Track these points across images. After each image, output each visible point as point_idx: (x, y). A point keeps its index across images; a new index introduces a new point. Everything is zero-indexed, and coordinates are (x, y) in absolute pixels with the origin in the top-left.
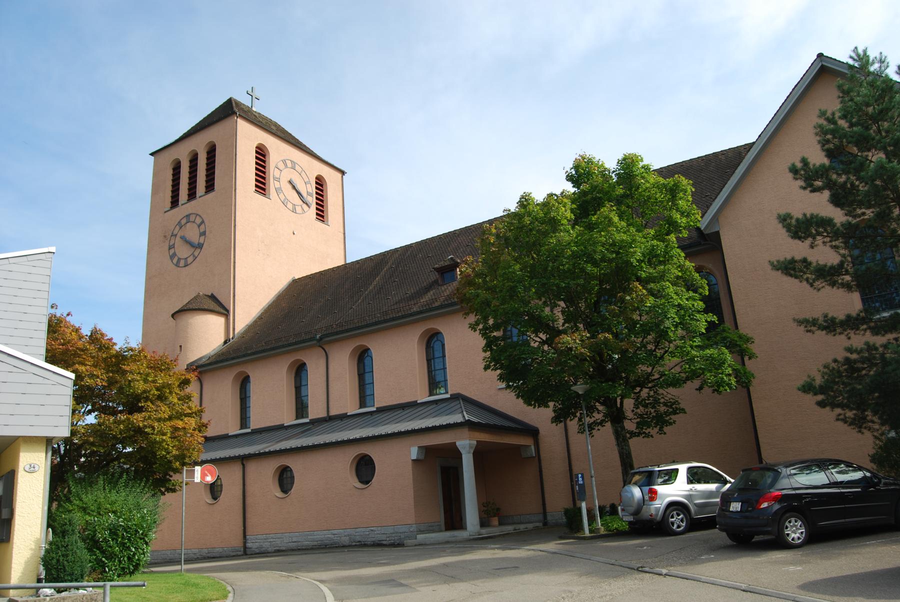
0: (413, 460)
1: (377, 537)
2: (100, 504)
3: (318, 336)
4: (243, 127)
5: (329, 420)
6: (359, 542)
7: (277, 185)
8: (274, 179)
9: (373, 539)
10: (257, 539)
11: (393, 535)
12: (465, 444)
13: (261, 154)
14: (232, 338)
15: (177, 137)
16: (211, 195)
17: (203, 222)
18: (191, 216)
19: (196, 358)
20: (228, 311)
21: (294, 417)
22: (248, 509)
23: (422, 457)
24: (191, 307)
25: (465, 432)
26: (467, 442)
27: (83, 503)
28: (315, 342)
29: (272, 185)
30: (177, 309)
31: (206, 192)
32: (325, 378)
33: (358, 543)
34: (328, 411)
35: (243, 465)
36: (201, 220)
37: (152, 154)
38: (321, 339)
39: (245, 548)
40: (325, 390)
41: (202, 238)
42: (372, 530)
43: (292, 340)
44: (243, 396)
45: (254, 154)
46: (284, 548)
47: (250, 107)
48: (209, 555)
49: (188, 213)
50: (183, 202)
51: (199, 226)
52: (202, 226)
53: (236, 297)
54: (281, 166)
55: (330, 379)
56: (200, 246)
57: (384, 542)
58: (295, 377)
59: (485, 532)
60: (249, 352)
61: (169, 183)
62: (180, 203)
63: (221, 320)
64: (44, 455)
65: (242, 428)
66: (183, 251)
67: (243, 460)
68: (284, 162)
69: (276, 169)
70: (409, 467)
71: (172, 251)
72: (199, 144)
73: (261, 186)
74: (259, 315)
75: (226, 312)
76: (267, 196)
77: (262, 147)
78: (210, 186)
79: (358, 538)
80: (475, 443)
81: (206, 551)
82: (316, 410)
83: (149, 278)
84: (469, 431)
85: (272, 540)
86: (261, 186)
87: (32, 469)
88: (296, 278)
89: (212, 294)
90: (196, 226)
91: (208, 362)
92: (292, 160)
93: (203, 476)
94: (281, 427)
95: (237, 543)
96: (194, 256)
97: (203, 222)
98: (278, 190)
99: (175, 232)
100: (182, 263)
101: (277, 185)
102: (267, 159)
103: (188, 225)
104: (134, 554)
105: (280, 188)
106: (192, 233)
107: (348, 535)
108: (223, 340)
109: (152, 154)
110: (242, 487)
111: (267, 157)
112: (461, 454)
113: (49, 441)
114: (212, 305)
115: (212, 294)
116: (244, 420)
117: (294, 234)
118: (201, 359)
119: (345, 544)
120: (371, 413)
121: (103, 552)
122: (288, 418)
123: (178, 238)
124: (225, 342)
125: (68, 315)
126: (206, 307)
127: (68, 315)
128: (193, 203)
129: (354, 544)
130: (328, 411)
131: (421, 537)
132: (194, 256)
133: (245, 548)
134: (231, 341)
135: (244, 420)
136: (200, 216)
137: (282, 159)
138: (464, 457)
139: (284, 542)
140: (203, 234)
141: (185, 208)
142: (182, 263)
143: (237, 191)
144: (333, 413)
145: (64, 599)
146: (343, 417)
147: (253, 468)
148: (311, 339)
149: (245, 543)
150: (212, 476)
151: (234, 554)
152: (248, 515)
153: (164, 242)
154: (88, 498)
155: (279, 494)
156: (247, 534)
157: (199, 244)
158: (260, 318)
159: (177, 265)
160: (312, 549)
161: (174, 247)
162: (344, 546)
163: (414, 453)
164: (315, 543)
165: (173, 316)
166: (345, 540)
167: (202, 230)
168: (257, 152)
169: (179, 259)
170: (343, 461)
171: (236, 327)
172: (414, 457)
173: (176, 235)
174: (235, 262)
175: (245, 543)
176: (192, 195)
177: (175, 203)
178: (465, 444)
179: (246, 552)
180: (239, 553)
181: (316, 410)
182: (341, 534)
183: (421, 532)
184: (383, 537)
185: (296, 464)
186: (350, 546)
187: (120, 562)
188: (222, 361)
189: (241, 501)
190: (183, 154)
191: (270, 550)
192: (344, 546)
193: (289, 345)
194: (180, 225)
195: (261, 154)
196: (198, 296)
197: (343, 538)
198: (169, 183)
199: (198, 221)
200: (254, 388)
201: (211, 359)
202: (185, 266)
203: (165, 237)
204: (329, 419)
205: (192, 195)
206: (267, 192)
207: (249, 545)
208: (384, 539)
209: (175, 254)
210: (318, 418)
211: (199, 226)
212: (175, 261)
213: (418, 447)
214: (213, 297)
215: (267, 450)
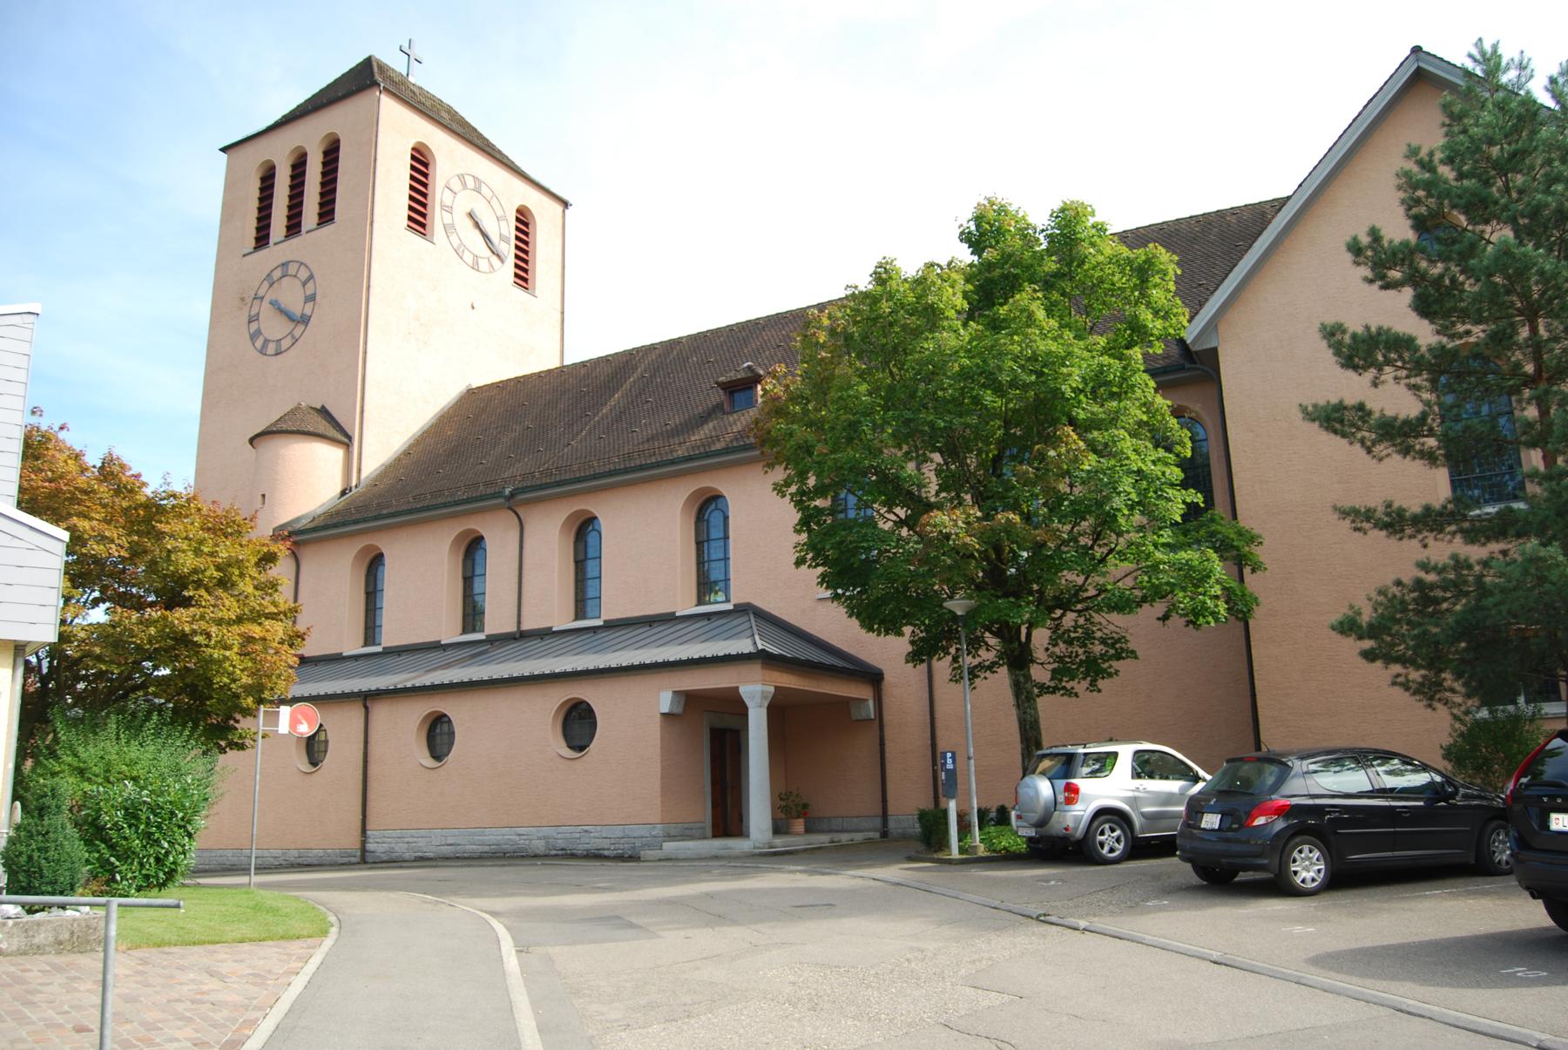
0: (662, 714)
3: (507, 491)
4: (391, 111)
6: (562, 849)
7: (447, 218)
8: (442, 207)
9: (587, 846)
10: (384, 837)
11: (623, 841)
12: (756, 690)
13: (421, 162)
14: (356, 487)
17: (311, 277)
20: (350, 438)
21: (460, 629)
23: (678, 710)
25: (756, 669)
28: (502, 500)
30: (259, 430)
31: (318, 224)
33: (560, 852)
34: (519, 622)
35: (366, 708)
36: (308, 274)
37: (224, 150)
38: (512, 495)
39: (364, 850)
42: (586, 831)
44: (371, 590)
45: (408, 161)
46: (431, 855)
48: (300, 861)
49: (284, 260)
51: (304, 284)
52: (310, 285)
53: (365, 414)
54: (456, 184)
55: (525, 567)
56: (305, 320)
59: (781, 843)
63: (334, 454)
64: (10, 671)
65: (366, 644)
66: (274, 327)
67: (367, 698)
68: (461, 177)
70: (658, 718)
71: (254, 326)
72: (310, 136)
73: (419, 218)
75: (346, 440)
76: (427, 237)
77: (423, 150)
78: (327, 214)
79: (561, 844)
80: (772, 689)
82: (497, 620)
84: (763, 668)
85: (411, 840)
86: (419, 218)
89: (323, 407)
90: (299, 284)
93: (294, 722)
95: (351, 842)
96: (293, 337)
97: (311, 277)
98: (449, 229)
99: (261, 293)
100: (271, 348)
101: (447, 218)
104: (167, 853)
105: (452, 226)
106: (292, 297)
107: (544, 838)
108: (339, 489)
109: (224, 150)
110: (362, 746)
111: (430, 167)
112: (746, 708)
114: (322, 426)
115: (323, 407)
116: (371, 631)
117: (473, 308)
118: (298, 519)
119: (538, 852)
120: (594, 629)
123: (266, 303)
124: (343, 493)
125: (62, 428)
126: (311, 430)
127: (62, 428)
128: (295, 241)
129: (554, 852)
130: (519, 622)
131: (669, 846)
132: (293, 337)
133: (364, 850)
134: (354, 491)
135: (371, 631)
136: (307, 267)
140: (311, 298)
141: (280, 249)
142: (271, 348)
143: (375, 225)
144: (527, 625)
145: (39, 924)
146: (545, 634)
149: (364, 843)
152: (371, 796)
153: (241, 309)
154: (89, 753)
155: (429, 762)
158: (407, 453)
159: (263, 351)
161: (258, 319)
163: (665, 702)
164: (486, 848)
165: (251, 441)
166: (539, 846)
167: (309, 292)
168: (413, 158)
169: (266, 341)
171: (363, 468)
175: (364, 843)
176: (294, 227)
177: (262, 239)
178: (756, 690)
179: (365, 859)
180: (353, 860)
181: (497, 620)
184: (605, 844)
185: (459, 711)
186: (546, 856)
187: (142, 865)
189: (360, 771)
190: (280, 153)
191: (407, 856)
192: (536, 856)
195: (421, 162)
196: (297, 408)
197: (536, 842)
199: (303, 274)
200: (391, 576)
202: (277, 354)
203: (242, 299)
204: (521, 636)
205: (294, 227)
207: (370, 846)
208: (606, 847)
209: (258, 333)
211: (304, 284)
212: (259, 343)
213: (674, 692)
214: (324, 412)
215: (409, 685)
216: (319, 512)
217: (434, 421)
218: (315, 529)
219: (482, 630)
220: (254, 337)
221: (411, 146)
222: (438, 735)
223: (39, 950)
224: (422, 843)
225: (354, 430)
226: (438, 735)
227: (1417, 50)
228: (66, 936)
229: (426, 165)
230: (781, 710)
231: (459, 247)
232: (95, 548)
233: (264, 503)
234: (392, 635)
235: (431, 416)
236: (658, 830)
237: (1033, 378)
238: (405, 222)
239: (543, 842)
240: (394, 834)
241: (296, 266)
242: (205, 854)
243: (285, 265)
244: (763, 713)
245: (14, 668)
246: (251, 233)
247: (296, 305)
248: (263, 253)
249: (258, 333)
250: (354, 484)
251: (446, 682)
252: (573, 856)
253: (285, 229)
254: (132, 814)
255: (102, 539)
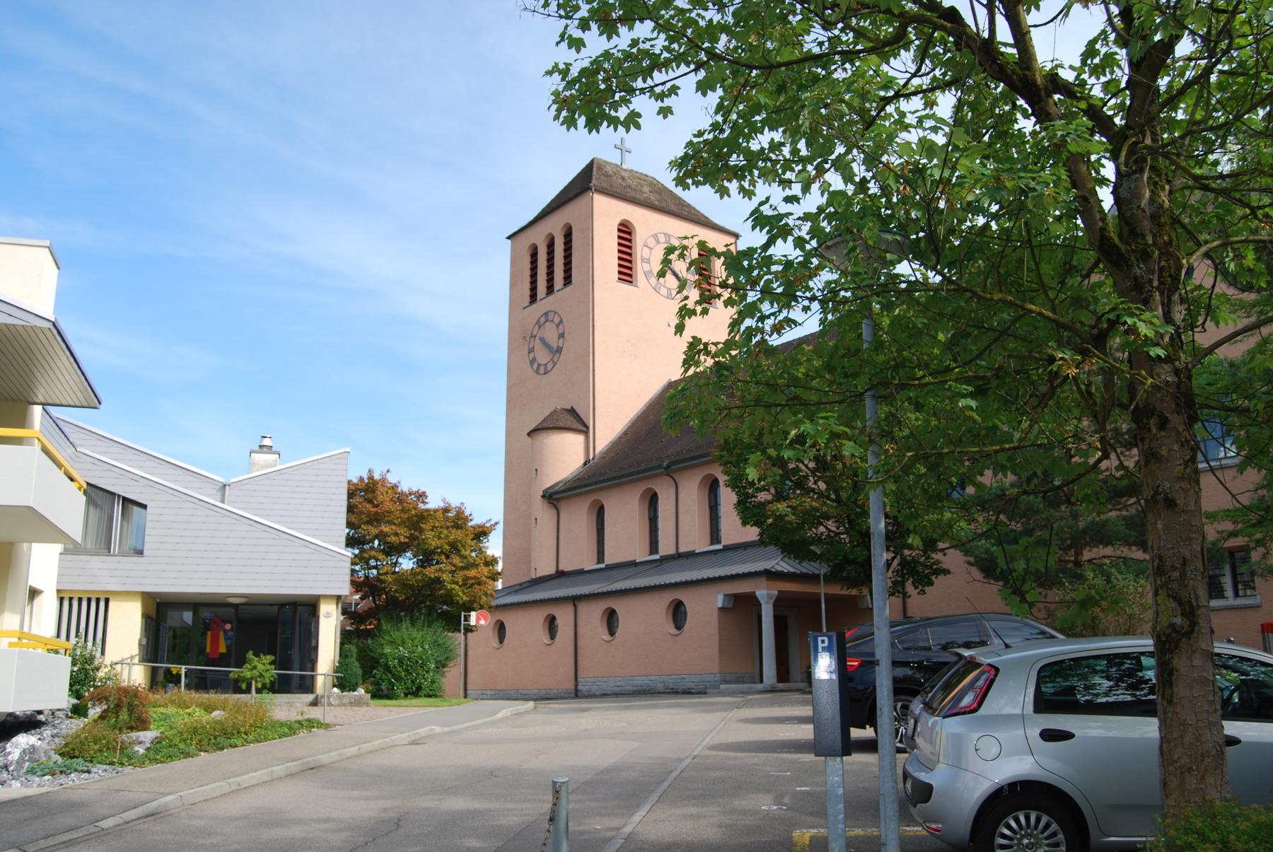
0: (720, 608)
1: (687, 685)
2: (404, 639)
3: (665, 464)
4: (600, 202)
5: (679, 557)
8: (643, 260)
9: (684, 687)
12: (765, 594)
13: (626, 231)
14: (593, 459)
15: (531, 218)
16: (569, 288)
17: (561, 321)
18: (549, 314)
19: (552, 484)
20: (587, 427)
21: (596, 561)
22: (580, 651)
23: (730, 605)
24: (546, 425)
25: (763, 581)
26: (765, 592)
27: (1242, 674)
28: (662, 470)
29: (640, 268)
30: (532, 428)
31: (564, 285)
32: (674, 511)
34: (677, 548)
35: (575, 606)
37: (509, 238)
38: (668, 467)
39: (576, 690)
40: (675, 524)
41: (561, 340)
42: (683, 678)
43: (643, 467)
44: (600, 527)
45: (616, 233)
46: (609, 692)
47: (619, 164)
48: (547, 696)
49: (545, 311)
50: (541, 297)
51: (558, 326)
52: (561, 327)
53: (596, 411)
54: (651, 242)
55: (680, 511)
56: (559, 350)
57: (693, 691)
58: (649, 508)
59: (781, 685)
60: (602, 478)
61: (527, 280)
62: (538, 298)
63: (578, 439)
64: (335, 606)
65: (712, 543)
66: (543, 356)
67: (575, 600)
68: (655, 236)
69: (645, 248)
70: (715, 613)
71: (532, 355)
72: (554, 225)
73: (626, 272)
74: (625, 429)
75: (585, 429)
78: (568, 280)
79: (671, 685)
80: (776, 593)
81: (544, 692)
82: (666, 548)
83: (511, 387)
84: (767, 580)
86: (626, 272)
87: (328, 615)
88: (673, 380)
89: (572, 408)
90: (555, 327)
91: (563, 488)
92: (666, 232)
93: (478, 619)
94: (634, 563)
95: (570, 685)
97: (561, 321)
99: (534, 333)
100: (542, 370)
102: (633, 238)
103: (547, 323)
104: (416, 679)
106: (550, 333)
108: (582, 462)
109: (509, 238)
110: (573, 628)
111: (633, 234)
112: (760, 605)
113: (339, 598)
114: (570, 421)
115: (572, 408)
116: (601, 557)
118: (557, 484)
121: (394, 676)
122: (642, 555)
123: (537, 340)
124: (585, 464)
125: (388, 471)
126: (562, 425)
127: (388, 471)
128: (551, 297)
130: (677, 548)
131: (723, 686)
133: (576, 690)
134: (592, 462)
135: (601, 557)
137: (653, 233)
138: (763, 607)
139: (609, 686)
140: (562, 336)
141: (544, 304)
142: (542, 370)
143: (595, 284)
144: (682, 549)
145: (344, 696)
146: (691, 555)
147: (584, 608)
148: (660, 466)
149: (576, 685)
150: (485, 620)
151: (567, 696)
152: (580, 658)
154: (396, 635)
156: (579, 676)
157: (558, 347)
158: (625, 433)
159: (537, 372)
160: (633, 694)
162: (659, 693)
163: (720, 601)
164: (636, 688)
165: (529, 434)
166: (660, 687)
167: (561, 332)
168: (619, 230)
169: (539, 365)
170: (658, 607)
171: (597, 446)
172: (720, 605)
173: (535, 336)
174: (594, 370)
175: (576, 685)
176: (550, 289)
177: (533, 298)
178: (765, 594)
179: (577, 694)
180: (572, 695)
181: (666, 548)
182: (657, 682)
183: (726, 682)
184: (692, 685)
185: (620, 606)
186: (664, 693)
187: (405, 683)
188: (575, 488)
190: (538, 237)
191: (597, 693)
192: (659, 693)
193: (639, 472)
194: (540, 325)
195: (626, 231)
196: (555, 411)
198: (528, 273)
199: (557, 320)
201: (567, 485)
202: (545, 374)
203: (524, 338)
204: (678, 556)
205: (550, 289)
206: (634, 280)
207: (580, 688)
209: (534, 359)
210: (622, 563)
211: (558, 326)
212: (535, 367)
213: (725, 595)
214: (572, 412)
215: (600, 591)
216: (570, 478)
217: (645, 408)
218: (564, 491)
219: (603, 562)
220: (532, 362)
221: (617, 223)
222: (611, 619)
223: (344, 705)
224: (604, 685)
225: (589, 418)
226: (611, 619)
227: (462, 504)
228: (353, 701)
229: (630, 234)
230: (781, 603)
231: (656, 285)
232: (393, 539)
233: (537, 474)
234: (610, 558)
235: (643, 405)
236: (718, 678)
237: (1050, 344)
238: (616, 276)
239: (662, 685)
240: (592, 680)
241: (552, 314)
242: (501, 693)
243: (546, 314)
244: (770, 607)
245: (337, 605)
246: (528, 293)
247: (553, 341)
248: (535, 306)
249: (534, 359)
250: (591, 457)
251: (694, 579)
252: (677, 693)
253: (546, 290)
254: (401, 662)
255: (396, 534)
